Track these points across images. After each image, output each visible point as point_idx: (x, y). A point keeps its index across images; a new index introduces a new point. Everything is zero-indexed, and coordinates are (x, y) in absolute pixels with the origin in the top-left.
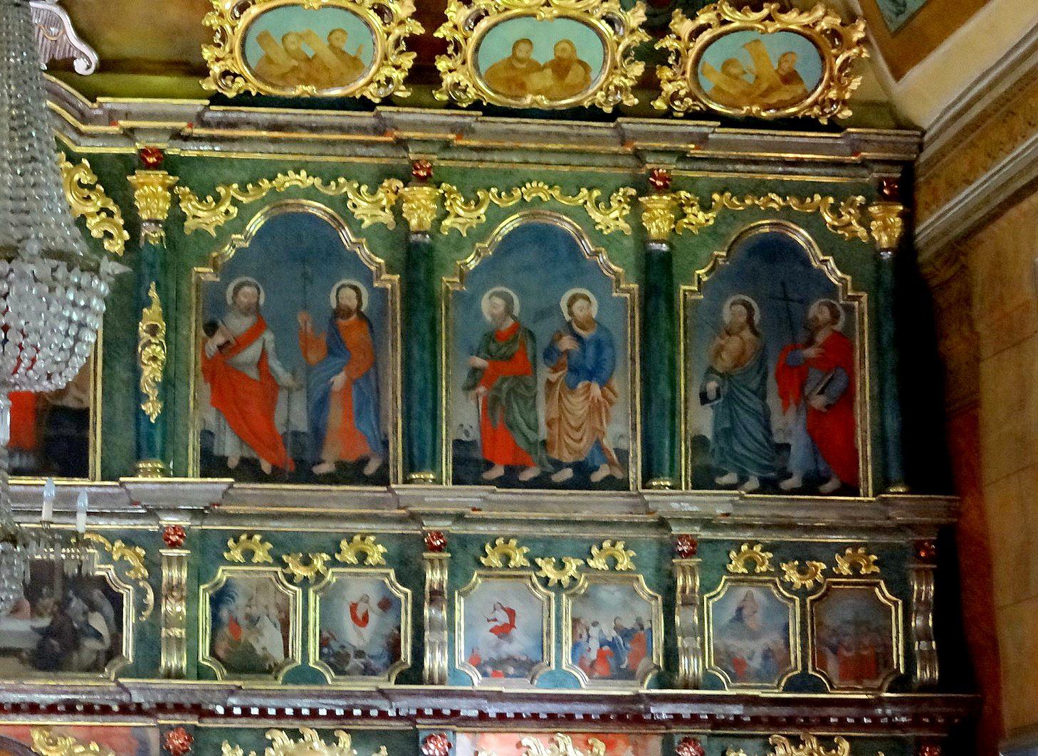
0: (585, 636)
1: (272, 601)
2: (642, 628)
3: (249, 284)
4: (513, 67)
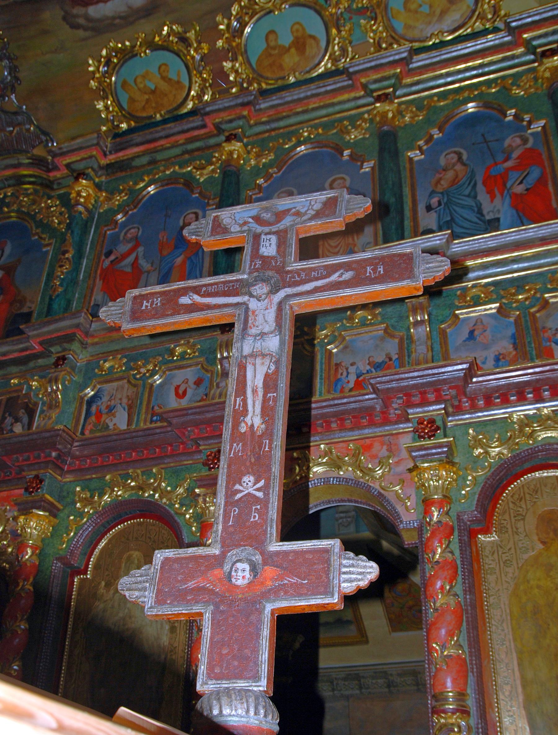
0: (345, 374)
1: (125, 395)
2: (390, 359)
3: (134, 228)
4: (271, 55)
